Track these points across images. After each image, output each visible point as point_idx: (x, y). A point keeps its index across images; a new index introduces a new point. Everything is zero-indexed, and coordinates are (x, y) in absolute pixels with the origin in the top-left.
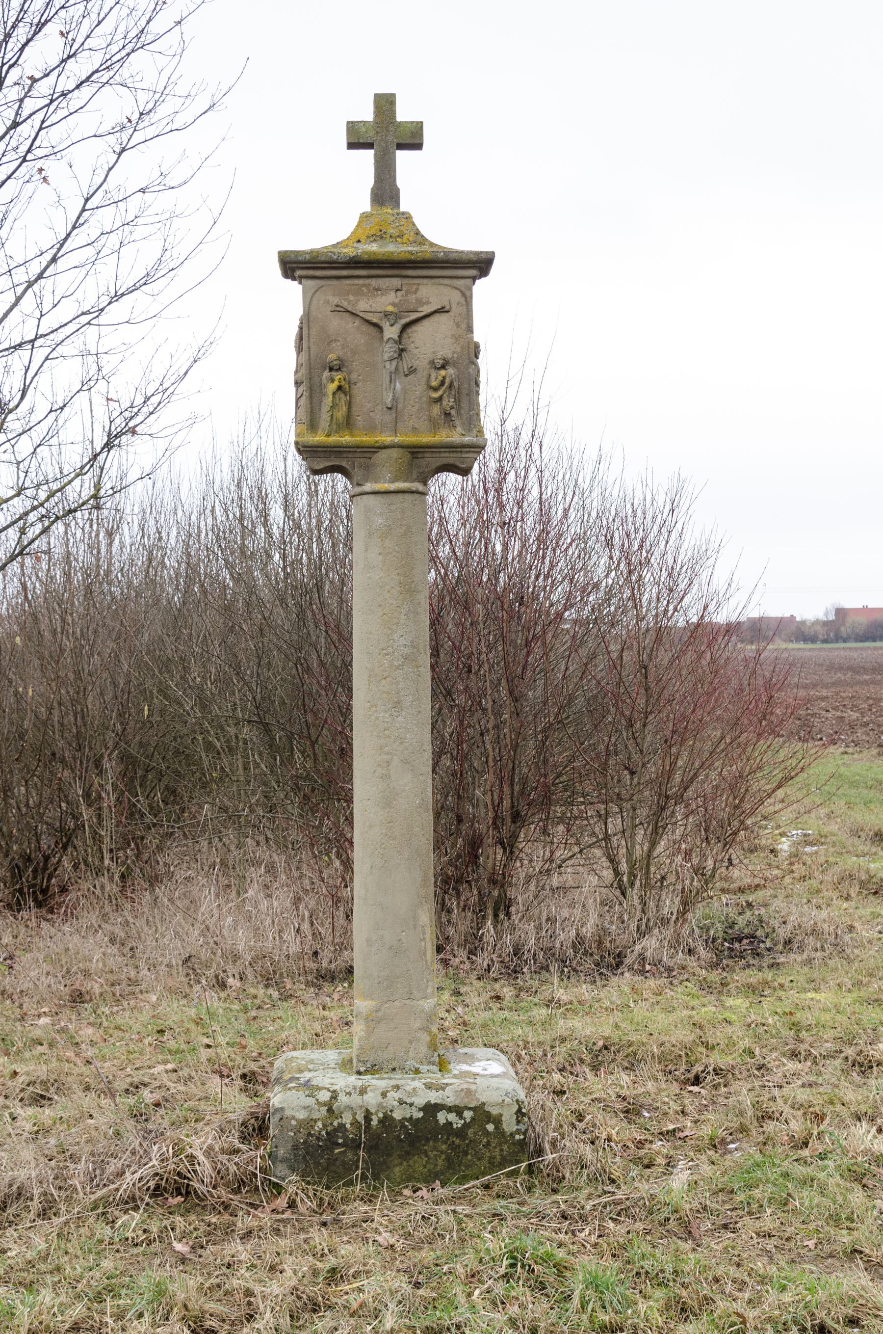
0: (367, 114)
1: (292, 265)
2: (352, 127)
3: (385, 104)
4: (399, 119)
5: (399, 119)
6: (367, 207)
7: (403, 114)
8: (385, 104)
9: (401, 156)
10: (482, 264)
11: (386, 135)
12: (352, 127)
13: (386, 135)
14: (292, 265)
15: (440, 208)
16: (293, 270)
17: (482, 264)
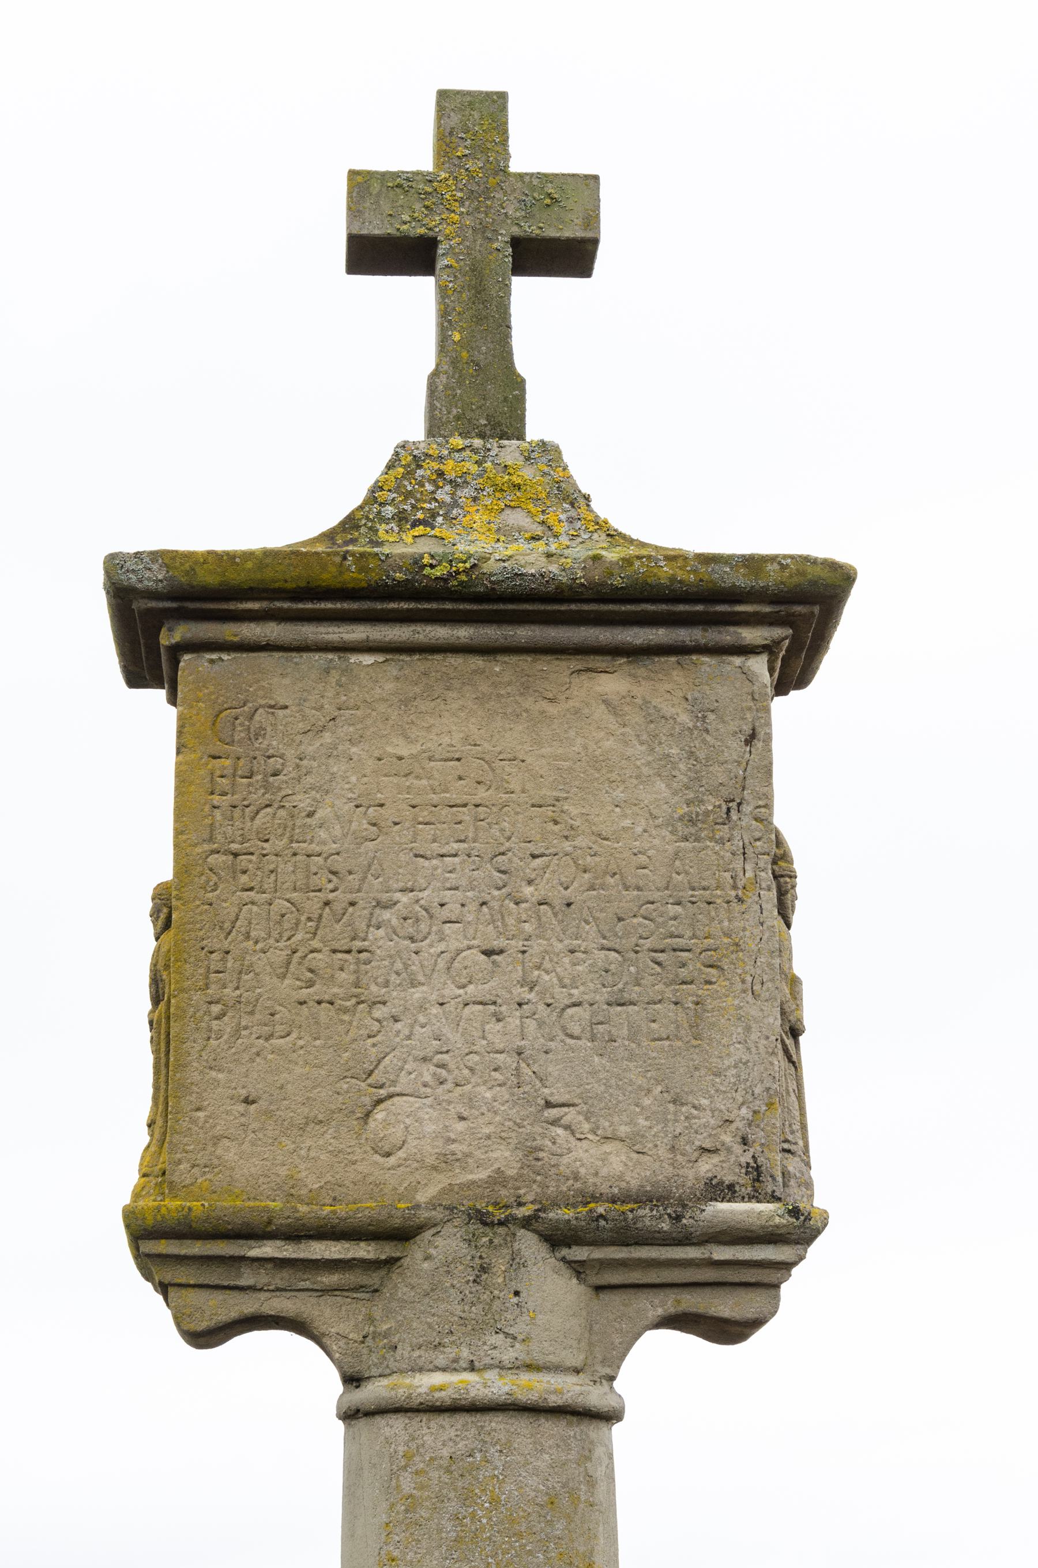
0: (414, 151)
1: (170, 618)
2: (362, 186)
3: (472, 122)
4: (515, 166)
5: (515, 166)
6: (416, 431)
7: (533, 149)
8: (472, 122)
9: (532, 297)
10: (789, 613)
11: (472, 227)
12: (362, 186)
13: (472, 227)
14: (170, 618)
15: (650, 430)
16: (155, 621)
17: (789, 613)
